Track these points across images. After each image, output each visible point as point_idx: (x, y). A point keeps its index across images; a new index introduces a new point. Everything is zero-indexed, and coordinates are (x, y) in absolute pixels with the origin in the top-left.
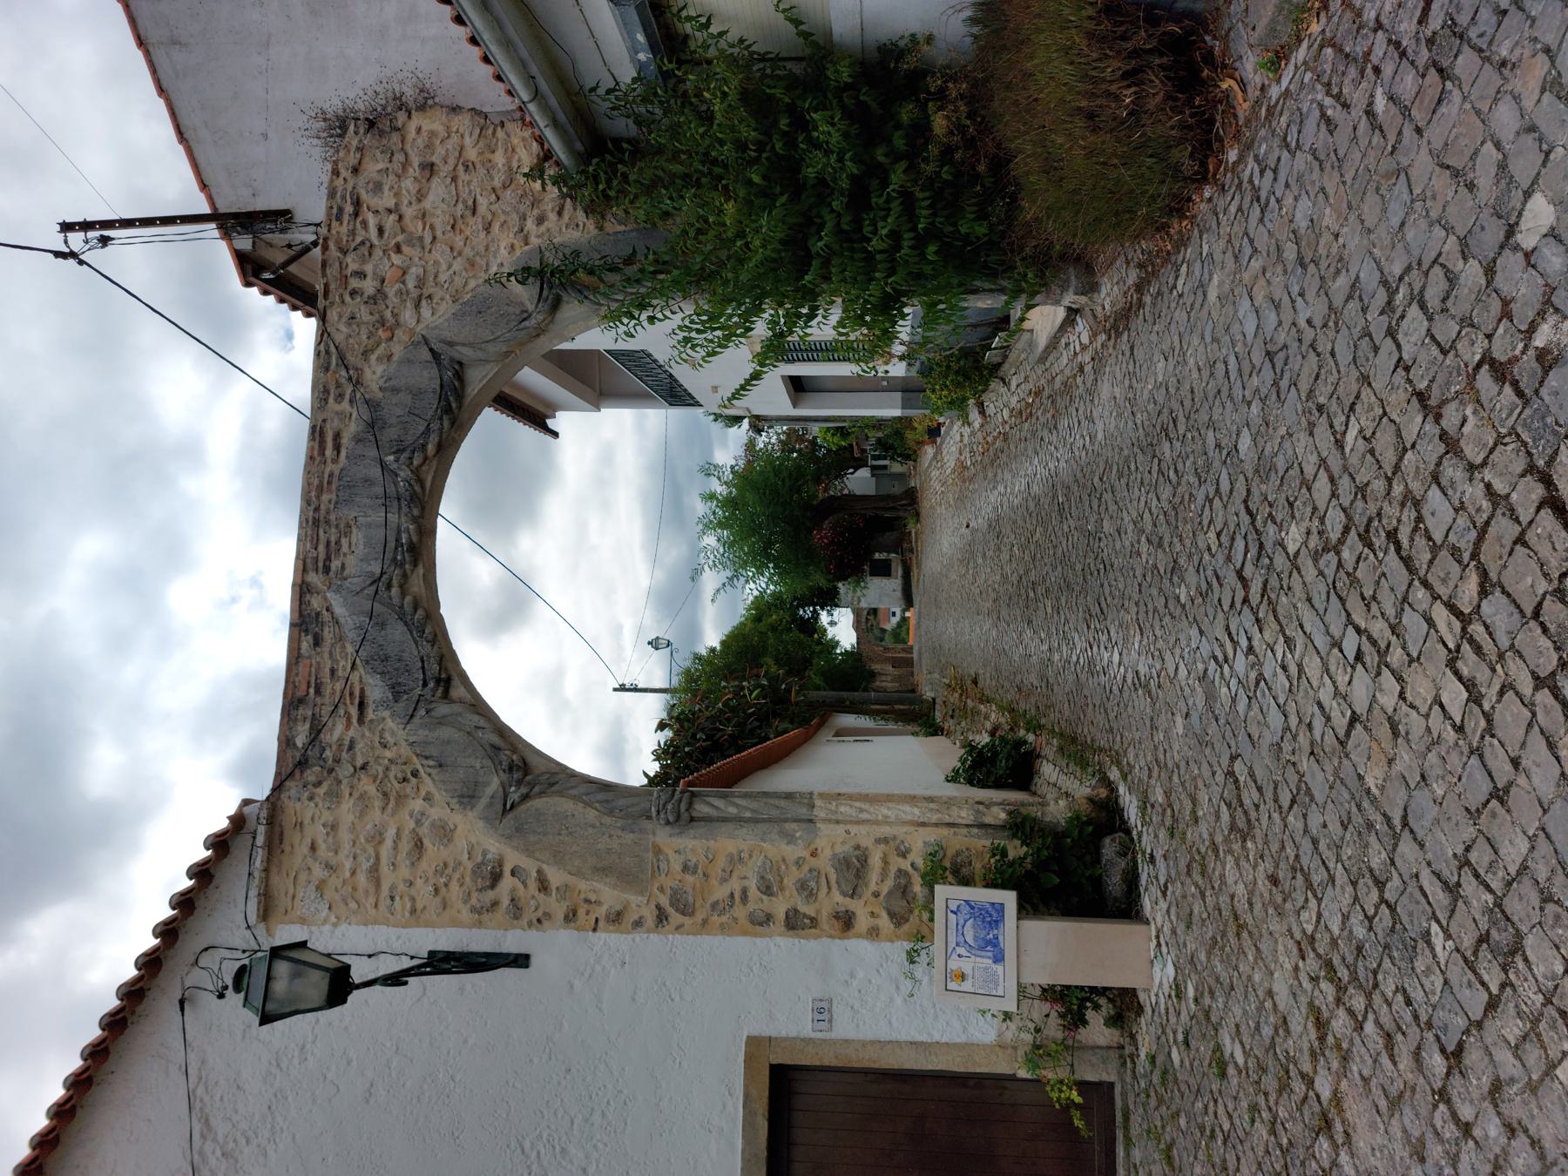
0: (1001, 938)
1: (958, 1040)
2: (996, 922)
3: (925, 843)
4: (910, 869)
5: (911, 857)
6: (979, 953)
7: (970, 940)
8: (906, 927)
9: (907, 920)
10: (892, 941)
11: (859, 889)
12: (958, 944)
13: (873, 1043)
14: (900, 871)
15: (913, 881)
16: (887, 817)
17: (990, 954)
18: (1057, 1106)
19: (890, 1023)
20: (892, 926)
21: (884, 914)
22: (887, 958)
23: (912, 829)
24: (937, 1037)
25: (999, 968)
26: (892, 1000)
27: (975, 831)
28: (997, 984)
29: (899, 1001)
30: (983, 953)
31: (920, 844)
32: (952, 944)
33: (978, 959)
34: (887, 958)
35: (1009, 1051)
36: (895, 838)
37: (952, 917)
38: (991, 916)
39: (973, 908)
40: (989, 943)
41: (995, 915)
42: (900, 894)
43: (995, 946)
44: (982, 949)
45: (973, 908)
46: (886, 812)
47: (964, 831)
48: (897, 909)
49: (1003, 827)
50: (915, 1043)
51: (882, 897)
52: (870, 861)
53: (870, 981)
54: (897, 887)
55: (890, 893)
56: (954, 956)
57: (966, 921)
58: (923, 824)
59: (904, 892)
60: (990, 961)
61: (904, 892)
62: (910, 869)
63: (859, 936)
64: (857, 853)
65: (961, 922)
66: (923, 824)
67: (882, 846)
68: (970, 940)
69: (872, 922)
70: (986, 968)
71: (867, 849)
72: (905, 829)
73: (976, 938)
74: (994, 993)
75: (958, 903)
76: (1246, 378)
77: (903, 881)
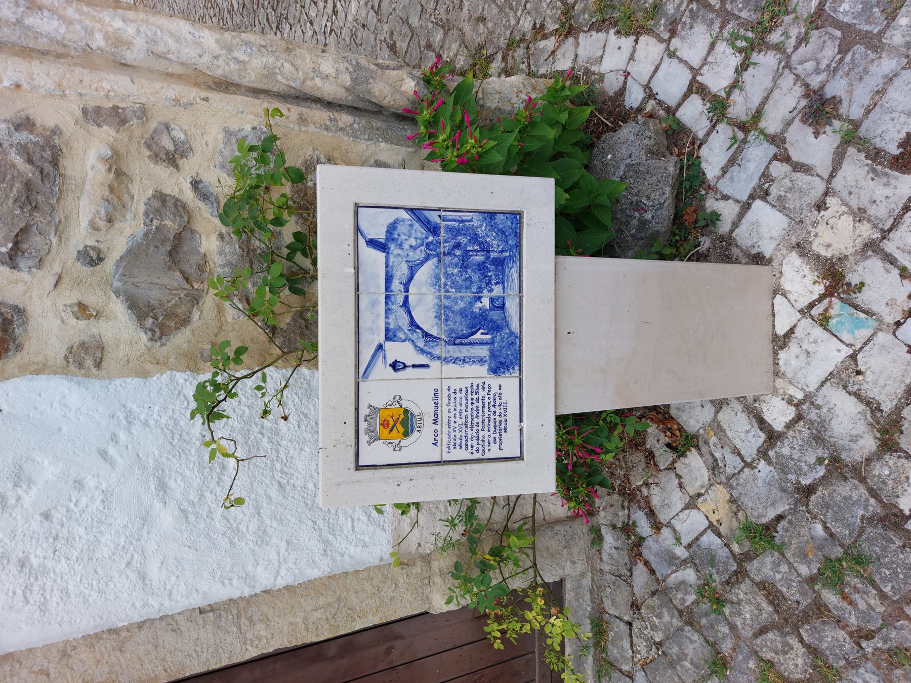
0: (511, 306)
1: (313, 573)
2: (500, 263)
3: (228, 133)
4: (188, 195)
5: (191, 166)
6: (454, 351)
7: (426, 318)
8: (181, 338)
9: (185, 322)
10: (144, 374)
11: (35, 241)
12: (390, 335)
13: (92, 640)
14: (161, 197)
15: (199, 226)
16: (118, 41)
17: (484, 352)
18: (498, 645)
19: (143, 577)
20: (144, 337)
21: (118, 308)
22: (130, 418)
23: (193, 94)
24: (265, 579)
25: (508, 384)
26: (146, 520)
27: (346, 119)
28: (501, 428)
29: (166, 518)
30: (464, 351)
31: (215, 136)
32: (374, 336)
33: (451, 369)
34: (130, 418)
35: (418, 569)
36: (143, 113)
37: (374, 259)
38: (486, 249)
39: (433, 229)
40: (479, 321)
41: (493, 241)
42: (161, 257)
43: (495, 328)
44: (457, 339)
45: (433, 229)
46: (118, 24)
47: (320, 115)
48: (155, 295)
49: (406, 117)
50: (212, 608)
51: (109, 264)
52: (69, 166)
53: (79, 484)
54: (154, 237)
55: (133, 255)
56: (381, 370)
57: (413, 271)
58: (225, 86)
59: (173, 253)
60: (482, 371)
61: (173, 253)
62: (188, 195)
63: (42, 369)
64: (23, 136)
65: (402, 271)
66: (225, 86)
67: (108, 132)
68: (426, 318)
69: (79, 329)
70: (473, 390)
71: (56, 131)
72: (173, 90)
73: (443, 312)
74: (494, 452)
75: (389, 216)
76: (327, 35)
77: (171, 224)
